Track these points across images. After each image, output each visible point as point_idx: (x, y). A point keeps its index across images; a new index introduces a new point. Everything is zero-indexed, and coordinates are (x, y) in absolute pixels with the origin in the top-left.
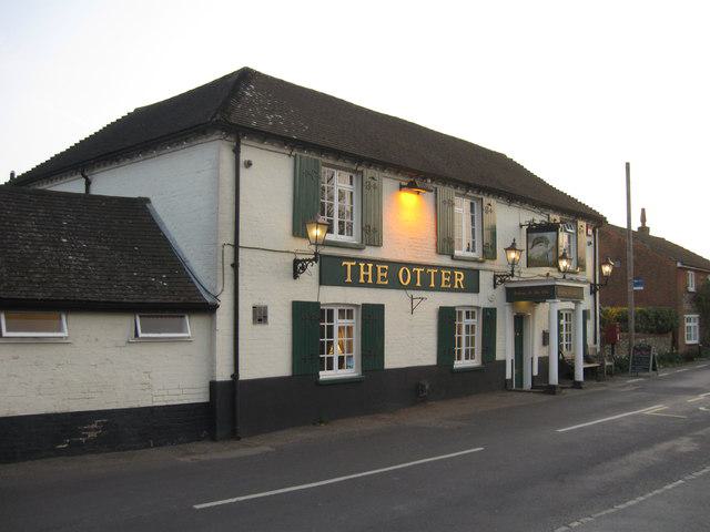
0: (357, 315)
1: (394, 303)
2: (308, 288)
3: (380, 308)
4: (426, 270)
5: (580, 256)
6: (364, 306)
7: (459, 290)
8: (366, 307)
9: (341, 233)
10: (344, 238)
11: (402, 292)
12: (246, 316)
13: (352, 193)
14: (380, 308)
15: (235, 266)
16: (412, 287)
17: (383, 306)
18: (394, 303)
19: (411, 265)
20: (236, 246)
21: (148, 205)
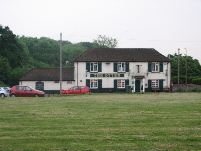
0: (97, 81)
1: (104, 80)
2: (89, 78)
3: (101, 80)
4: (40, 86)
5: (37, 84)
6: (159, 80)
7: (119, 77)
8: (98, 80)
9: (95, 70)
10: (95, 71)
11: (106, 78)
12: (79, 81)
13: (53, 100)
14: (101, 80)
15: (77, 76)
16: (107, 77)
17: (129, 80)
18: (104, 80)
19: (107, 74)
20: (78, 74)
21: (24, 38)
